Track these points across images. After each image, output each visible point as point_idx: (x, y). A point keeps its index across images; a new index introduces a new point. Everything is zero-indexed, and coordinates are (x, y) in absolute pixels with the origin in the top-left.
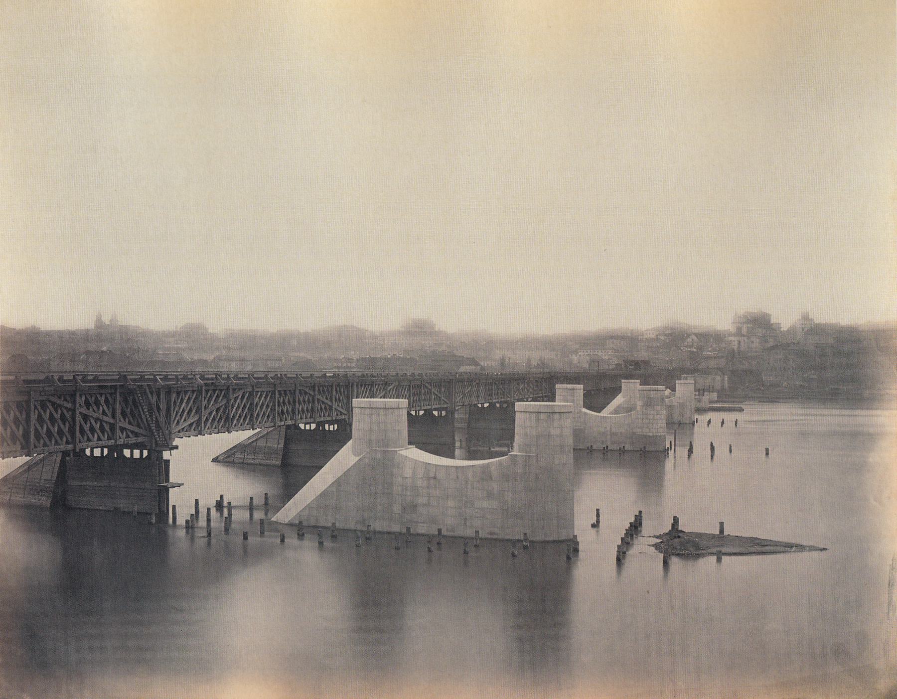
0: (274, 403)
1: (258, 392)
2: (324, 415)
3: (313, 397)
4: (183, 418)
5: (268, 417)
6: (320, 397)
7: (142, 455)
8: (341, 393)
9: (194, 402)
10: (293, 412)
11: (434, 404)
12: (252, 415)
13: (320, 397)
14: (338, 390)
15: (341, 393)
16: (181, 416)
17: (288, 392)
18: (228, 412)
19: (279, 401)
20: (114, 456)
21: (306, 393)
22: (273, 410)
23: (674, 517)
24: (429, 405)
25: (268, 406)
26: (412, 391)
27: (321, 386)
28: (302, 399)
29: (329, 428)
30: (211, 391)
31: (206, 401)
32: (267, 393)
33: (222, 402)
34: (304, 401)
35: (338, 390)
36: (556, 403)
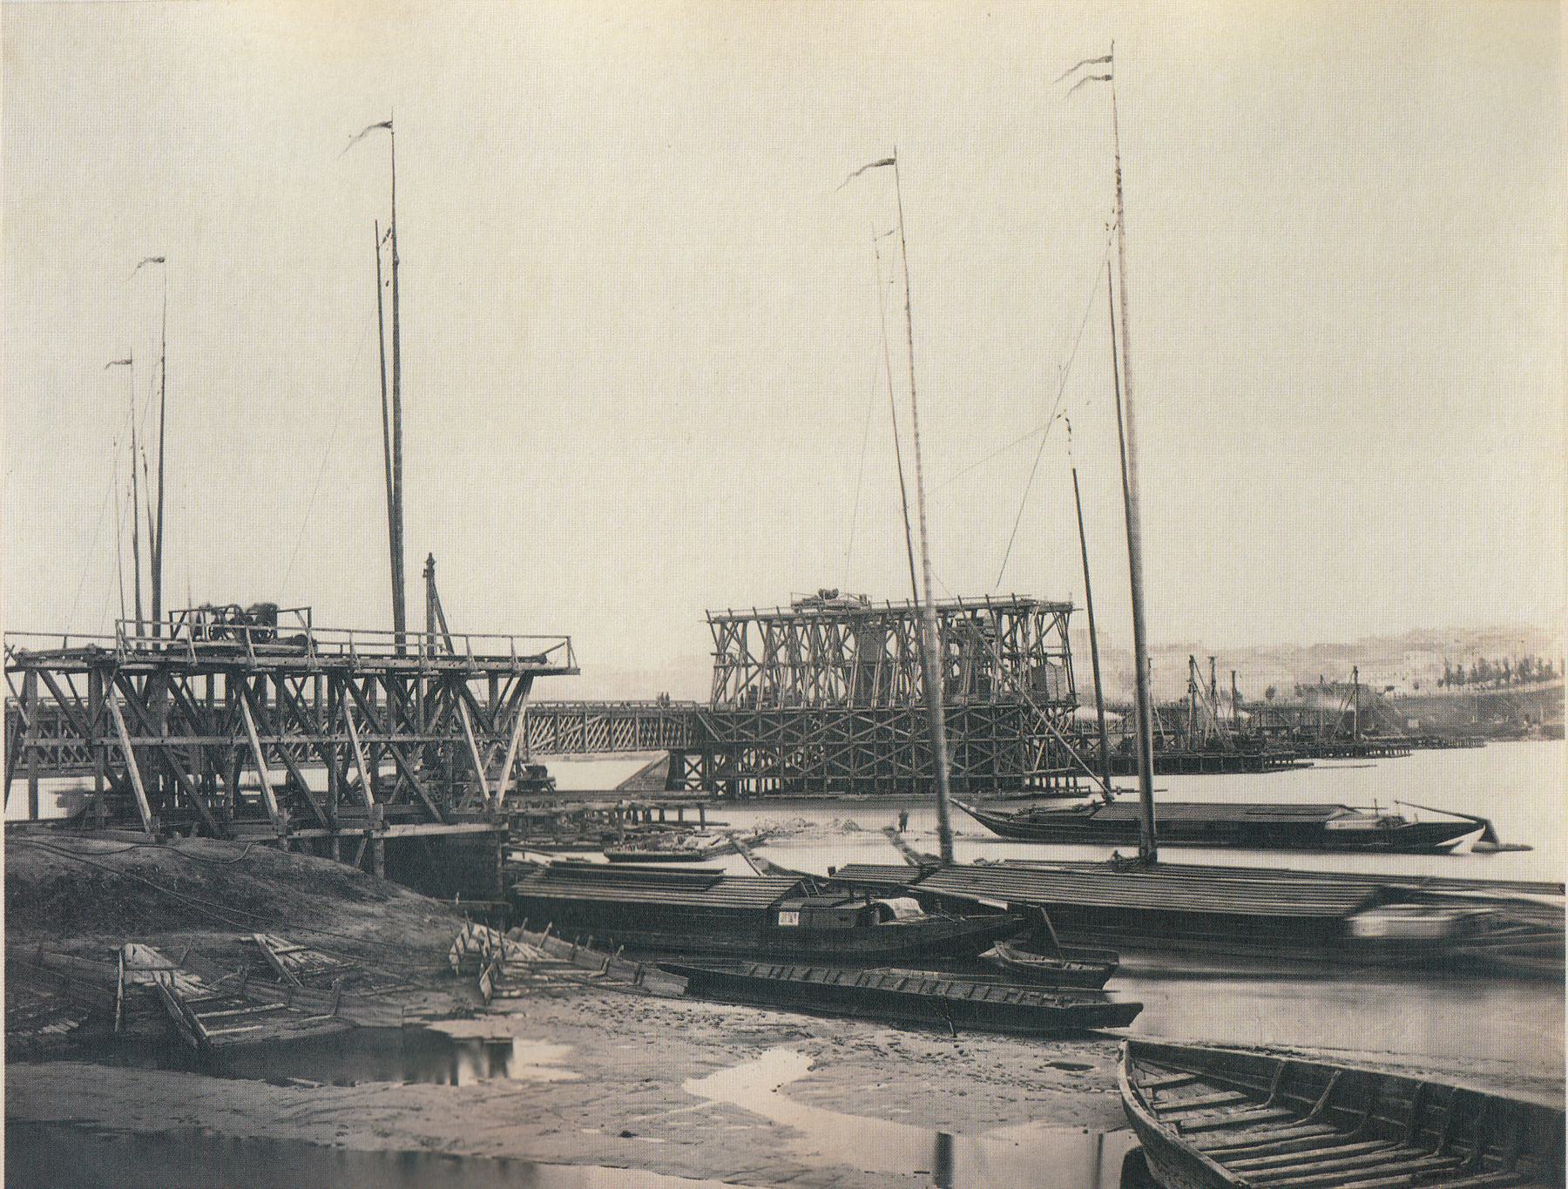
5: (629, 741)
25: (628, 732)
34: (647, 730)
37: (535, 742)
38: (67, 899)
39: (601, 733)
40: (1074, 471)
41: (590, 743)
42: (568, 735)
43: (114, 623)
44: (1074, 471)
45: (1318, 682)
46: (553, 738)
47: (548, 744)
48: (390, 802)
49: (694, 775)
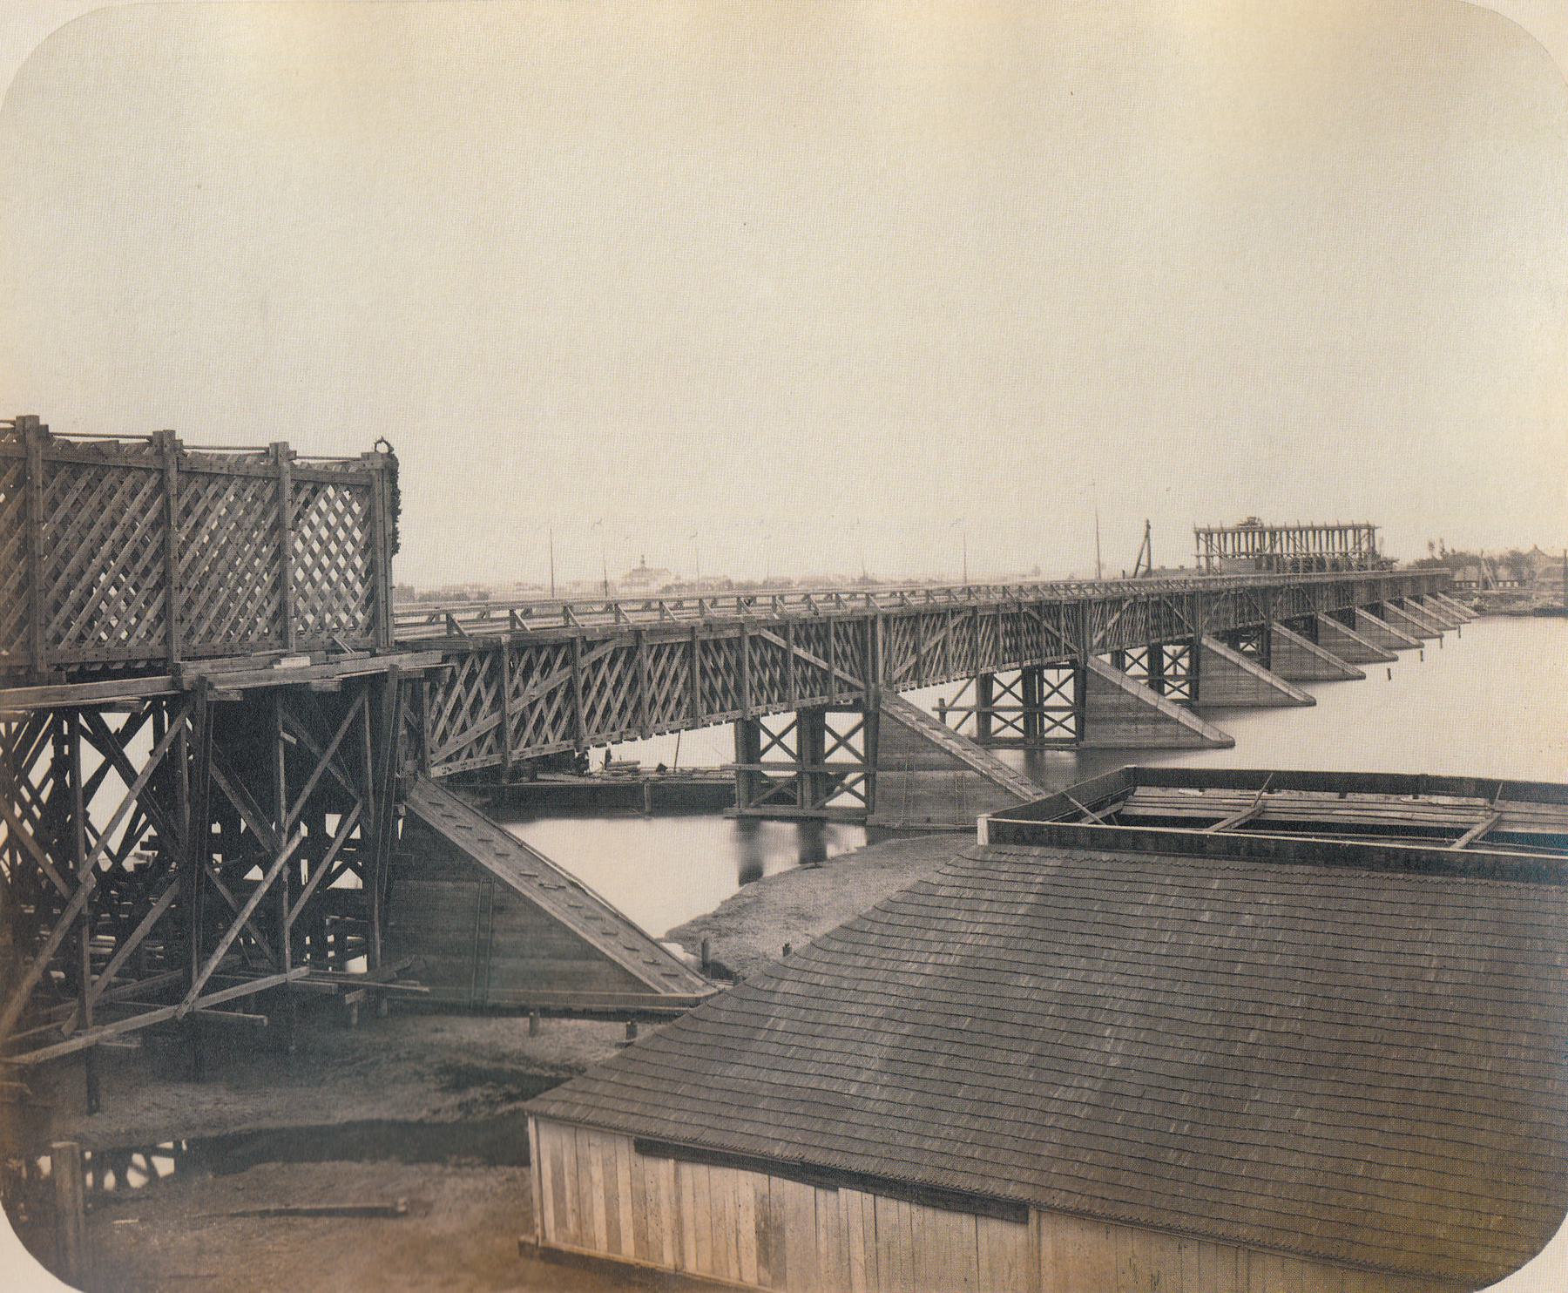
0: (691, 669)
1: (652, 646)
2: (721, 706)
3: (785, 652)
4: (459, 723)
5: (679, 703)
6: (801, 652)
7: (857, 765)
8: (848, 642)
9: (625, 664)
10: (739, 689)
11: (1046, 656)
12: (574, 715)
13: (801, 652)
14: (841, 633)
15: (848, 642)
16: (452, 718)
17: (711, 647)
18: (642, 689)
19: (751, 660)
20: (51, 855)
21: (767, 643)
22: (689, 687)
23: (787, 945)
24: (1015, 661)
25: (675, 678)
26: (1002, 627)
27: (840, 623)
28: (756, 660)
29: (811, 726)
30: (548, 649)
31: (650, 661)
32: (672, 649)
33: (558, 676)
34: (716, 671)
35: (841, 633)
36: (1354, 635)
37: (444, 736)
38: (484, 1103)
39: (600, 694)
40: (1390, 678)
41: (589, 718)
42: (532, 706)
43: (379, 438)
44: (1390, 678)
45: (1120, 575)
46: (494, 719)
47: (480, 741)
48: (1313, 613)
49: (1008, 700)
